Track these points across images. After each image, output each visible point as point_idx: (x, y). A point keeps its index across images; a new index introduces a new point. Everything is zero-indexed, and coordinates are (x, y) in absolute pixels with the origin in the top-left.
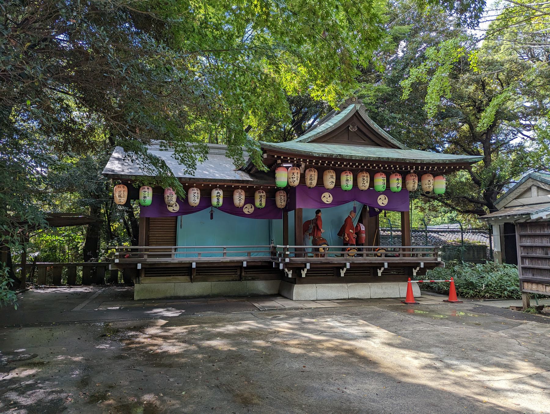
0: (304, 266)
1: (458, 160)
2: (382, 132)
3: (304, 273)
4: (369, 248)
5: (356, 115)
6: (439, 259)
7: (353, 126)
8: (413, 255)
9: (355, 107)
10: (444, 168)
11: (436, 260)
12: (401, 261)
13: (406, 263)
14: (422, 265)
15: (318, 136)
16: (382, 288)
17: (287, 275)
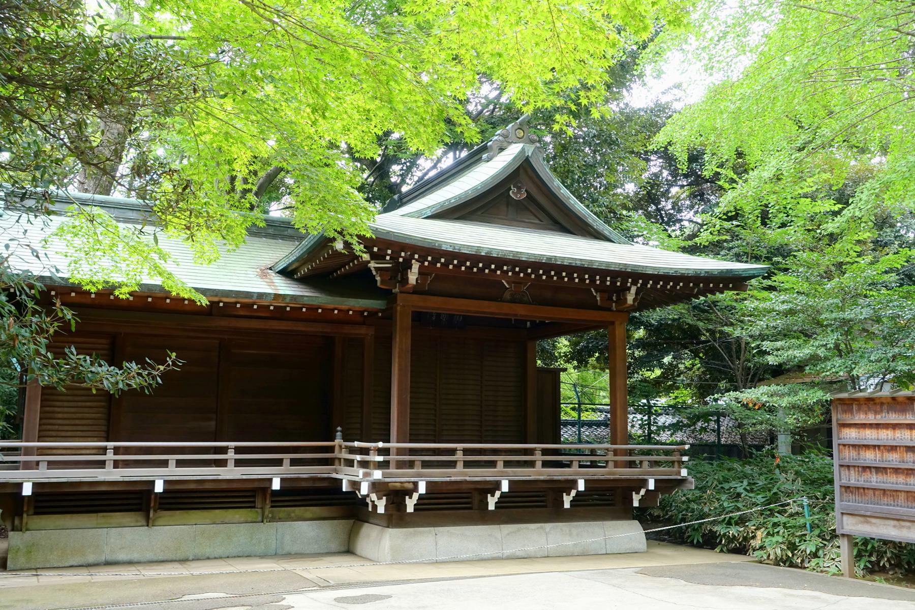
0: (411, 486)
1: (722, 271)
2: (579, 207)
3: (410, 504)
4: (626, 450)
5: (523, 170)
6: (684, 472)
7: (519, 189)
8: (631, 464)
9: (523, 149)
10: (696, 285)
11: (679, 473)
12: (612, 477)
13: (559, 481)
14: (651, 485)
15: (447, 206)
16: (570, 535)
17: (375, 507)
